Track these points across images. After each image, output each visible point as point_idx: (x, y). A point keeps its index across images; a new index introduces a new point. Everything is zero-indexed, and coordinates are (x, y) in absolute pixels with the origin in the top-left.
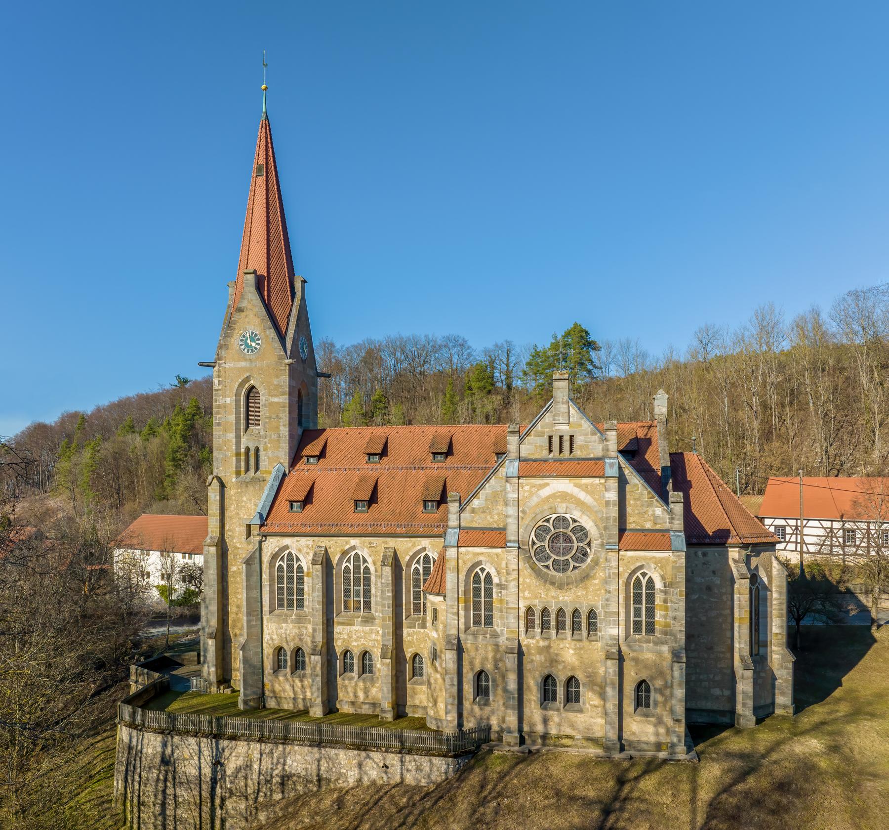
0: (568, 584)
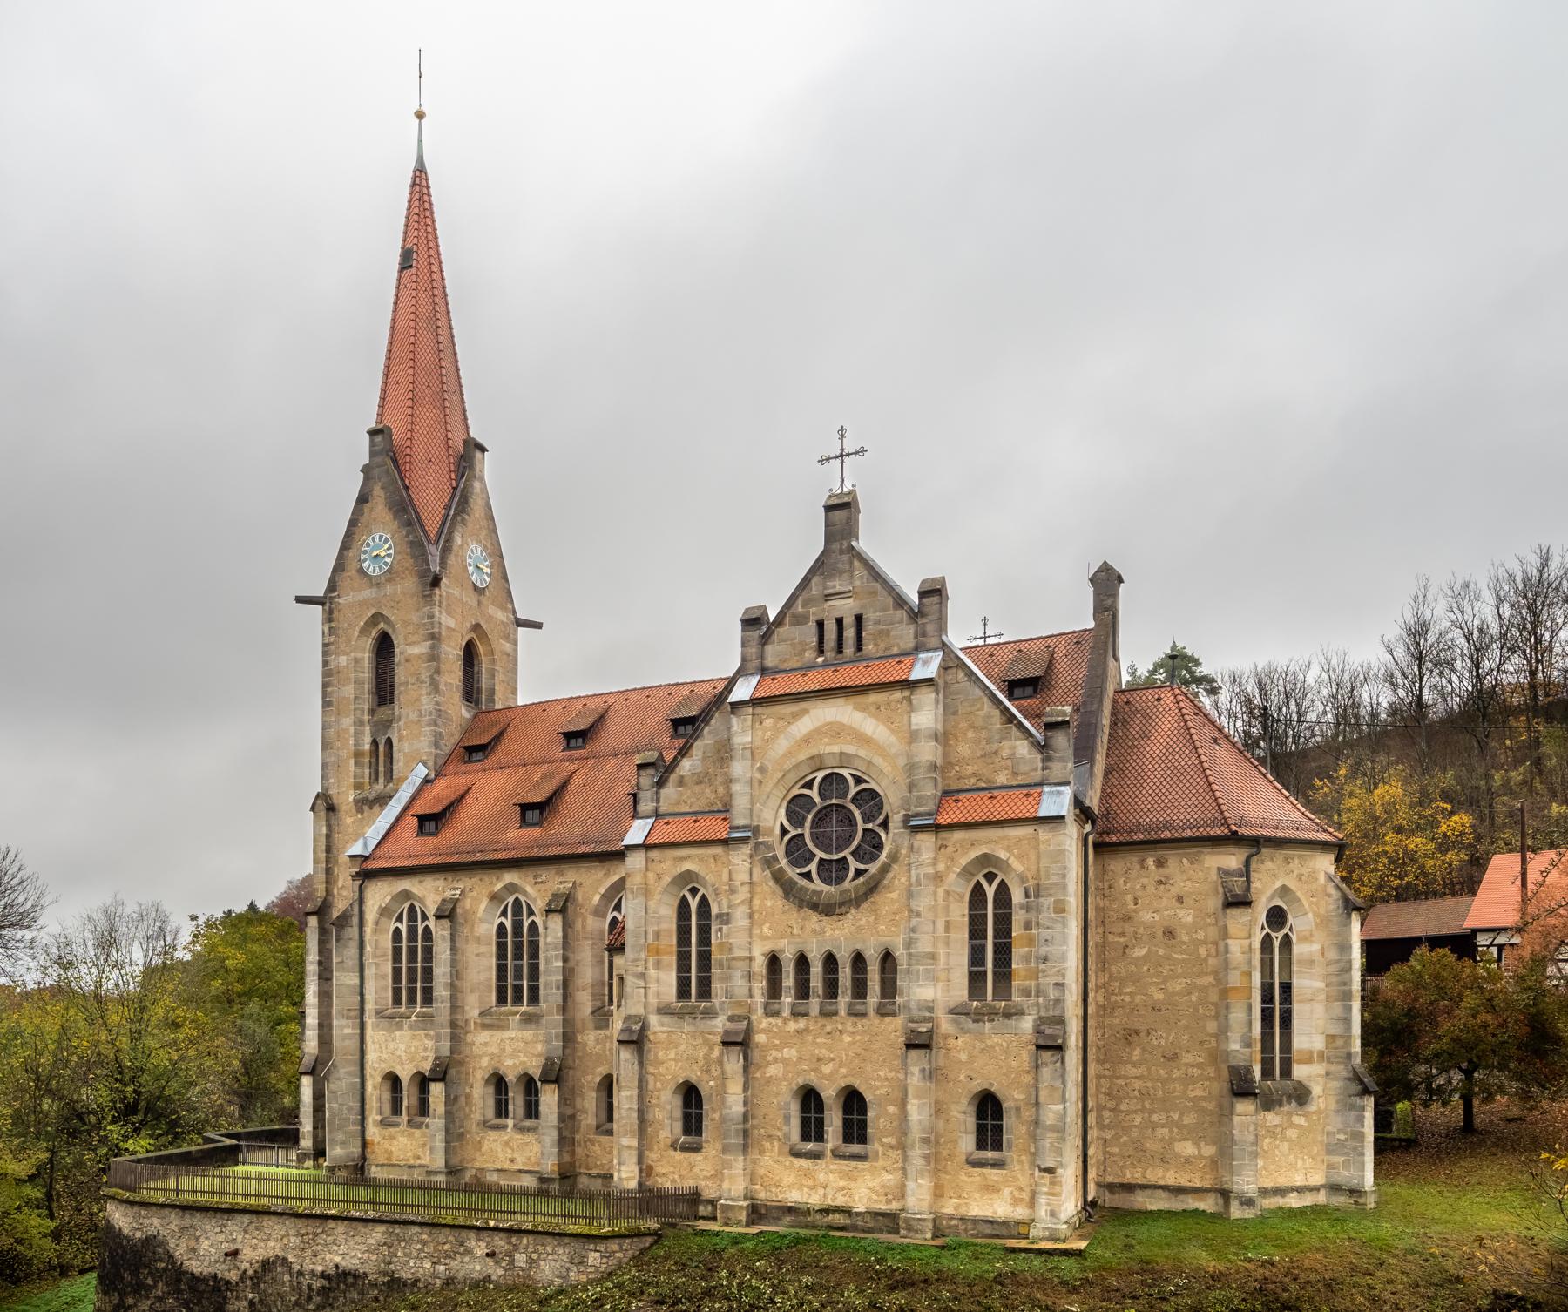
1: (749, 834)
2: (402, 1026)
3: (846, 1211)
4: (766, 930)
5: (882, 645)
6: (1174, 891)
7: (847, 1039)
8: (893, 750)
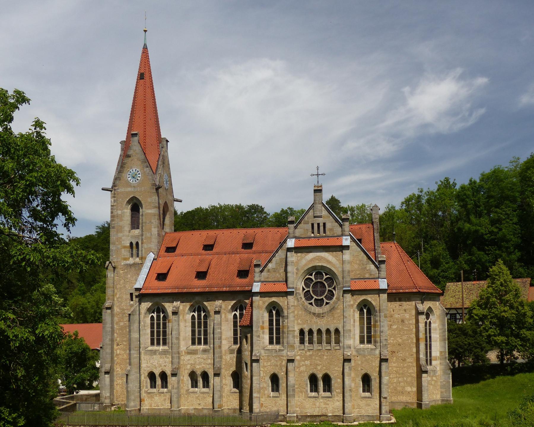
2: (156, 353)
4: (299, 321)
5: (332, 233)
6: (404, 308)
7: (325, 357)
8: (338, 266)
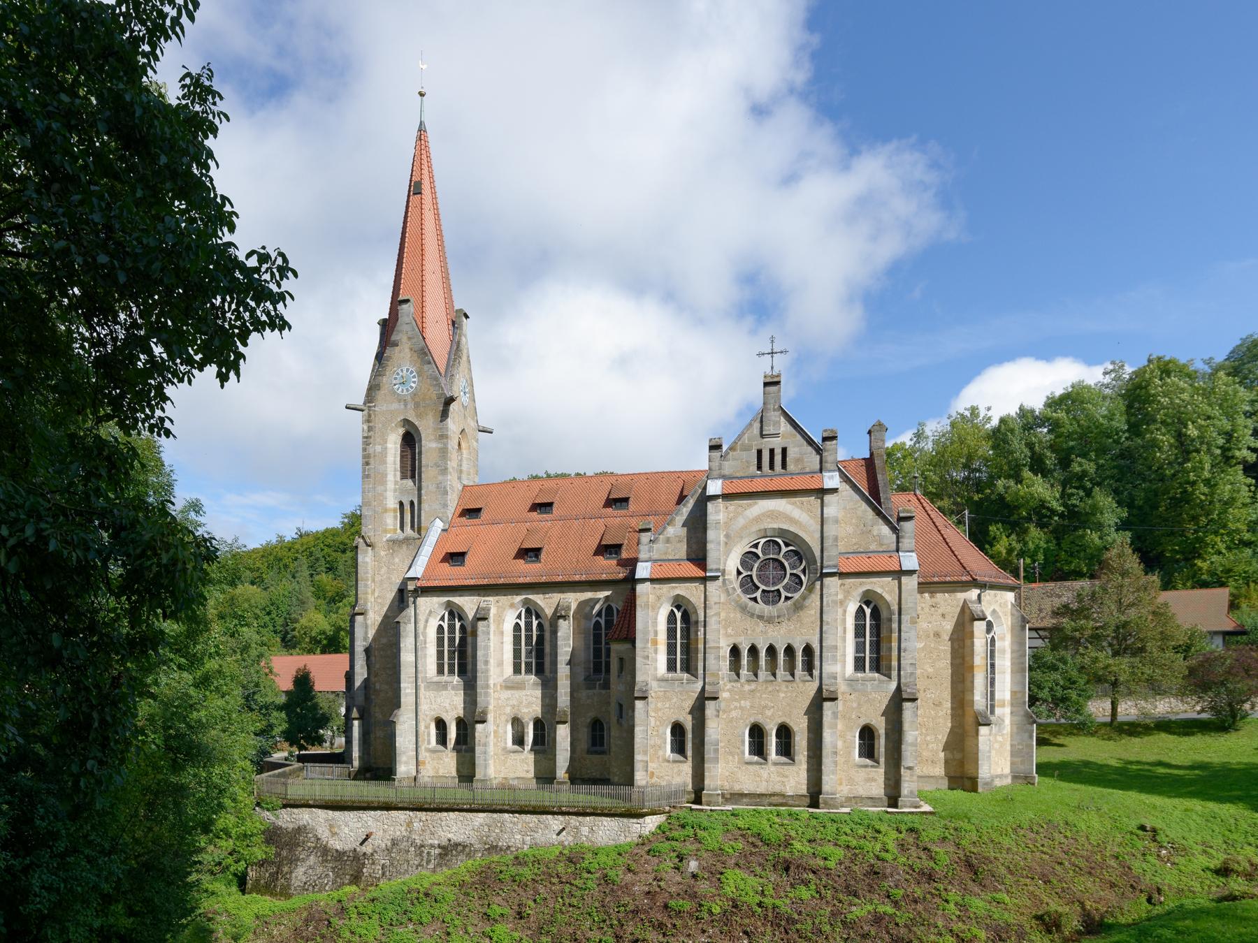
0: (778, 617)
1: (719, 574)
3: (783, 796)
6: (940, 611)
